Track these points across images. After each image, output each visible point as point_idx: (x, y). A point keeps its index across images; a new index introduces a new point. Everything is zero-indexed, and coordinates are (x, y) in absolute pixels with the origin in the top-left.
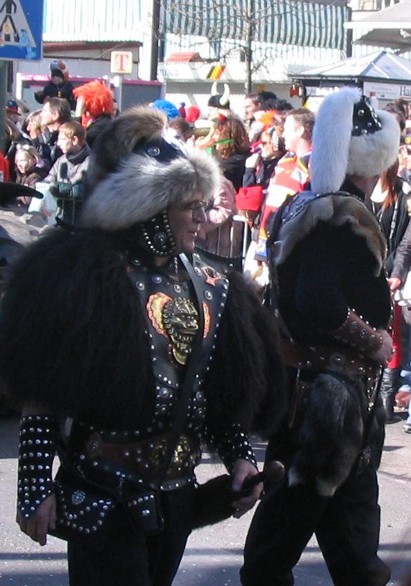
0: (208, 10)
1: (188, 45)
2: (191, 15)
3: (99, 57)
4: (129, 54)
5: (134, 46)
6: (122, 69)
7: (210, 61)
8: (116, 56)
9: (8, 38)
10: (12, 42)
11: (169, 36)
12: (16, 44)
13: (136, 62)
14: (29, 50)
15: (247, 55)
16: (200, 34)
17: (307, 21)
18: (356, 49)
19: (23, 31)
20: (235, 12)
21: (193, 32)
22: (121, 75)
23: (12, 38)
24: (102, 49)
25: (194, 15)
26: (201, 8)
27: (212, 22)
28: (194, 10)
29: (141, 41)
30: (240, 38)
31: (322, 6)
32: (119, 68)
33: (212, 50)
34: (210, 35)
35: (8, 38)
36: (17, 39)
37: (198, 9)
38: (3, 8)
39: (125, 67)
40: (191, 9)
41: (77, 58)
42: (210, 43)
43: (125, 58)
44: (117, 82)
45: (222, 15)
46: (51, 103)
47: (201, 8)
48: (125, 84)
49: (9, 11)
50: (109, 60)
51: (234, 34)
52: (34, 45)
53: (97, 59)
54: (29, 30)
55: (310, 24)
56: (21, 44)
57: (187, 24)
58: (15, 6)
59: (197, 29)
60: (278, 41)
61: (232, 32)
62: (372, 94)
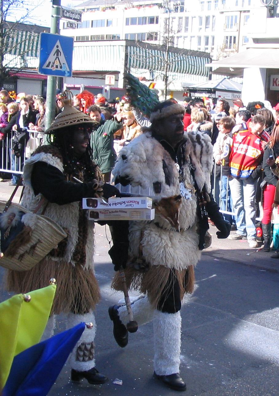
0: (149, 58)
1: (139, 73)
2: (141, 60)
3: (101, 77)
4: (113, 77)
5: (116, 73)
6: (110, 83)
7: (150, 80)
8: (108, 77)
9: (57, 67)
10: (59, 69)
11: (132, 69)
12: (61, 69)
13: (117, 80)
14: (66, 72)
15: (166, 79)
16: (145, 68)
17: (190, 63)
18: (214, 76)
19: (63, 64)
20: (161, 59)
21: (193, 74)
22: (110, 85)
23: (59, 67)
24: (102, 74)
25: (143, 60)
26: (146, 57)
27: (151, 63)
28: (143, 58)
29: (119, 71)
30: (157, 70)
31: (199, 58)
32: (109, 82)
33: (151, 77)
34: (150, 69)
35: (57, 67)
36: (61, 67)
37: (144, 58)
38: (55, 53)
39: (111, 82)
40: (141, 57)
41: (85, 78)
42: (150, 73)
43: (111, 78)
44: (108, 88)
45: (155, 61)
46: (181, 128)
47: (146, 57)
48: (111, 90)
49: (58, 55)
50: (105, 79)
51: (133, 65)
52: (69, 70)
53: (100, 79)
54: (66, 64)
55: (192, 65)
56: (63, 70)
57: (140, 64)
58: (60, 53)
59: (144, 66)
60: (185, 73)
61: (156, 67)
62: (220, 96)
